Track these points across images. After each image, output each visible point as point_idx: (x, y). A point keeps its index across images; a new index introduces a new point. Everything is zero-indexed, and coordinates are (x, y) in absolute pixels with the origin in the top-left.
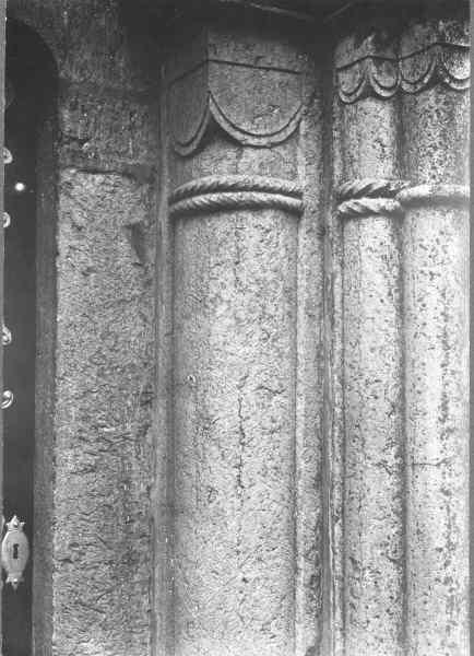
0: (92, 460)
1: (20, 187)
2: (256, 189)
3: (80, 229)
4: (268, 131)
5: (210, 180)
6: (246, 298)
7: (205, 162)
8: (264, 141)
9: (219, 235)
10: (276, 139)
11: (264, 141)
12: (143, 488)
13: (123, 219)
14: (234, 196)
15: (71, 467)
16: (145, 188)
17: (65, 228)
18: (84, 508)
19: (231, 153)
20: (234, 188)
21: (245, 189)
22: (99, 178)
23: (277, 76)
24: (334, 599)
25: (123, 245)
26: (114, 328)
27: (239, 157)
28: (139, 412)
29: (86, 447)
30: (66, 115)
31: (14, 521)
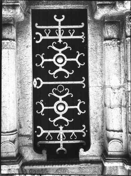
0: (26, 96)
1: (36, 132)
2: (8, 135)
3: (29, 127)
4: (5, 144)
5: (12, 136)
6: (8, 120)
7: (14, 138)
8: (6, 142)
9: (12, 128)
10: (4, 143)
11: (6, 142)
12: (19, 92)
13: (23, 129)
14: (11, 133)
15: (30, 95)
16: (20, 134)
17: (31, 127)
18: (27, 89)
19: (11, 140)
20: (11, 135)
21: (9, 135)
22: (27, 134)
23: (3, 152)
24: (10, 2)
25: (23, 125)
26: (23, 114)
27: (10, 139)
28: (20, 102)
29: (27, 98)
30: (32, 142)
31: (35, 87)
